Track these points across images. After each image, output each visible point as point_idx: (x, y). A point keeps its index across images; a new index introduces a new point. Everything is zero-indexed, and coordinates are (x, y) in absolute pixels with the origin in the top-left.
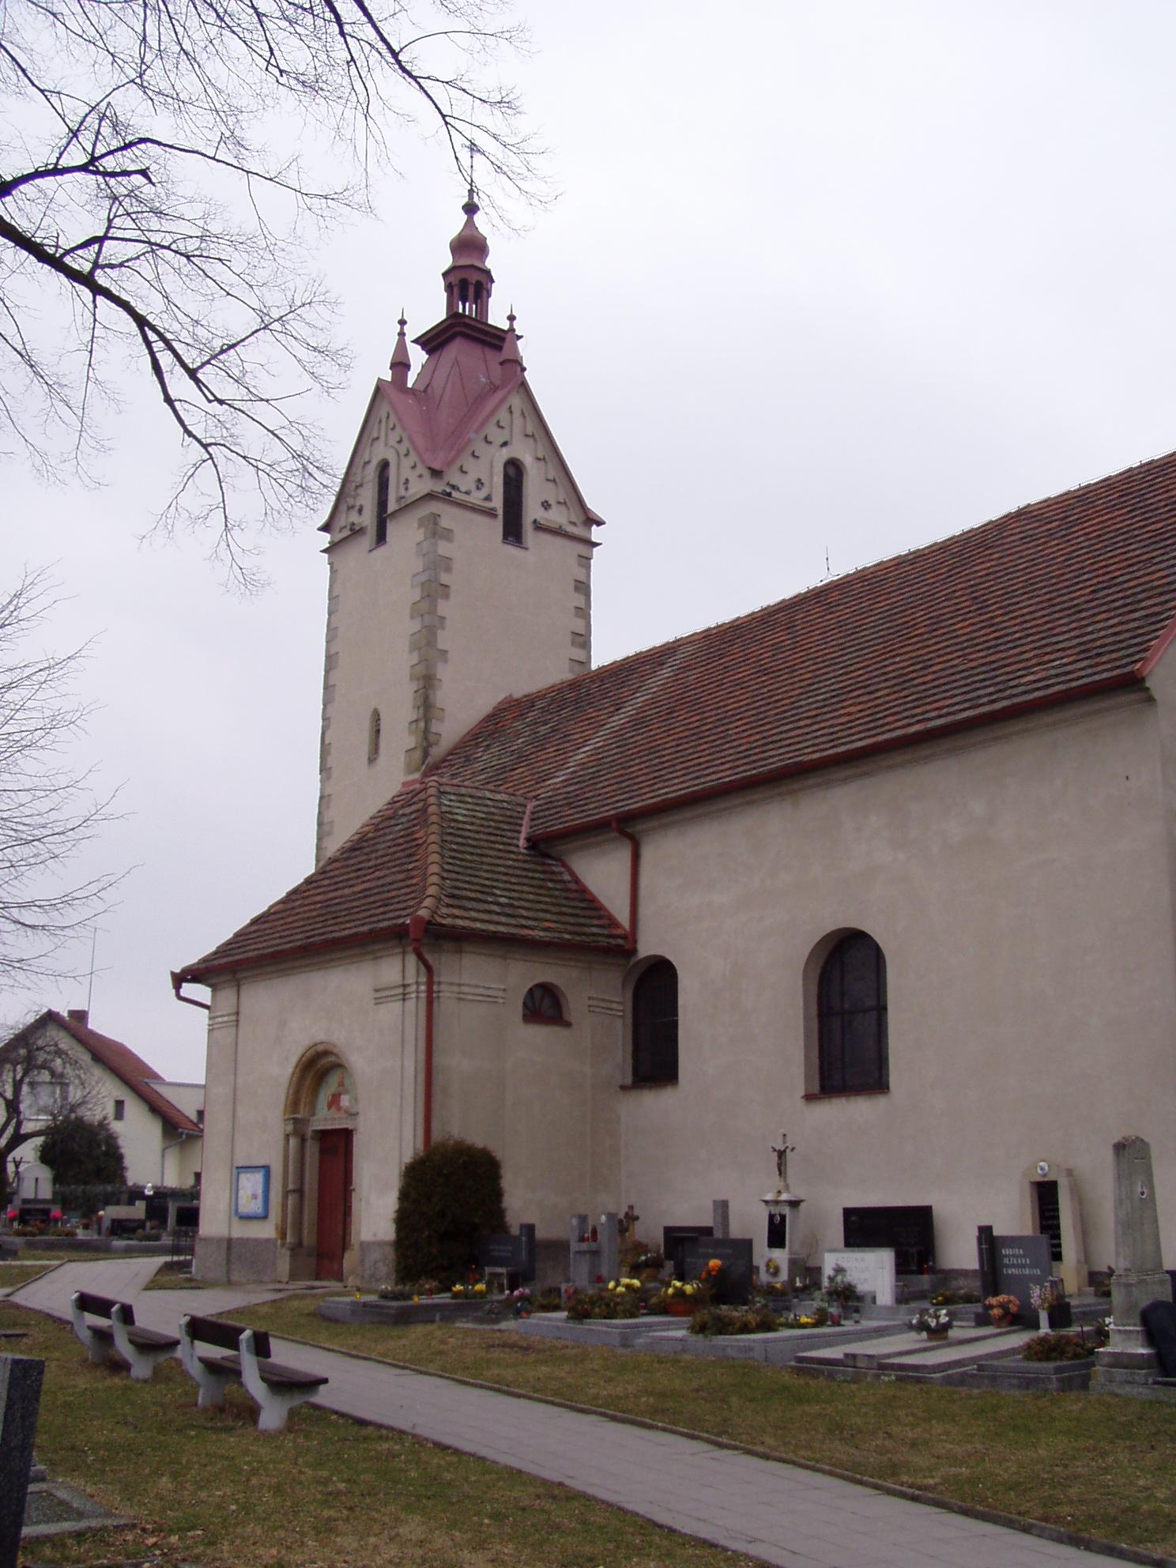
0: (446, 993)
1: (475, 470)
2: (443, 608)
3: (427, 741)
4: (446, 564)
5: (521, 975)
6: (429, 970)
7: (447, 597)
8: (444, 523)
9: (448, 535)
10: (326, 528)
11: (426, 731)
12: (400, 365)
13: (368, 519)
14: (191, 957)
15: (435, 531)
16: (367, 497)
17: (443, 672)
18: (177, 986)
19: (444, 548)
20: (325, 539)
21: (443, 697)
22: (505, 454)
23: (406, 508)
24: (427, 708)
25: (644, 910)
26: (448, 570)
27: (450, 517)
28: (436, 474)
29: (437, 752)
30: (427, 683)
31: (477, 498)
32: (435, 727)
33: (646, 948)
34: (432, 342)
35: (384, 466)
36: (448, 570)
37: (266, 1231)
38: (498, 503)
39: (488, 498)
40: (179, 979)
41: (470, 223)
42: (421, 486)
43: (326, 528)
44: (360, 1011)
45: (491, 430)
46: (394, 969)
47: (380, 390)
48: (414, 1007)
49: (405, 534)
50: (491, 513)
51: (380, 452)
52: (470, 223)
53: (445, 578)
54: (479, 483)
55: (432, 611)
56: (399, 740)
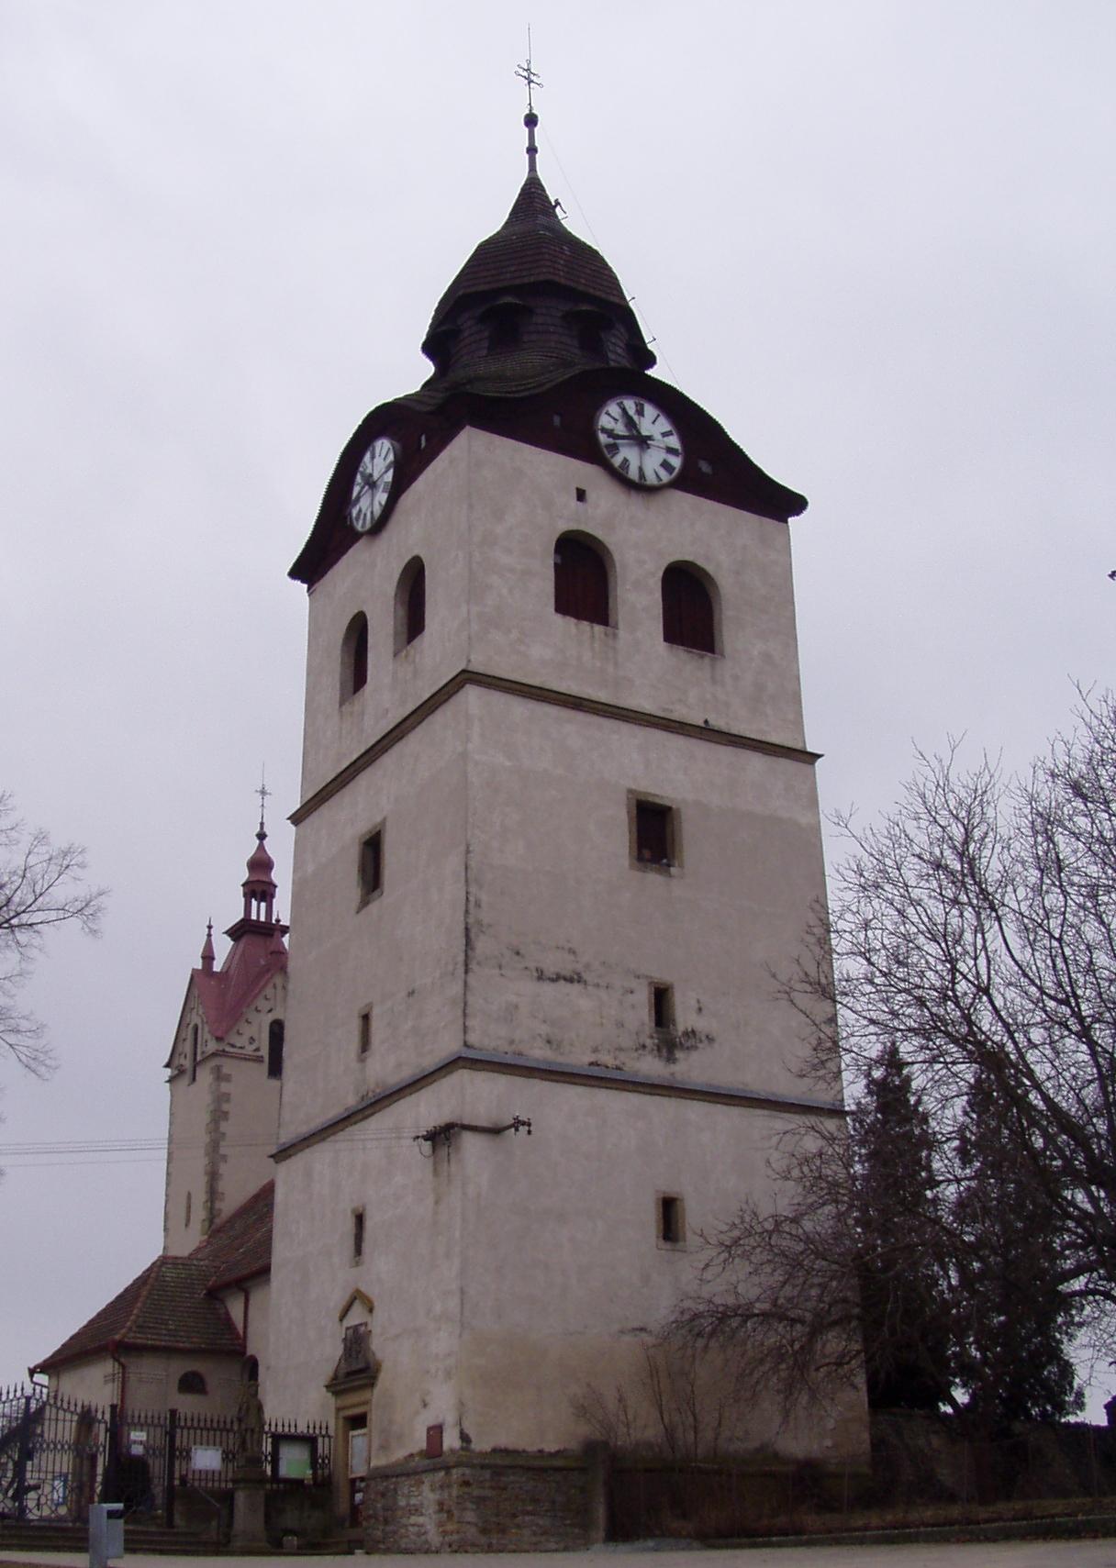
0: (132, 1379)
1: (248, 1031)
2: (224, 1127)
3: (212, 1214)
4: (226, 1097)
5: (179, 1367)
6: (123, 1367)
7: (226, 1119)
8: (225, 1070)
9: (228, 1078)
10: (167, 1066)
11: (212, 1209)
12: (208, 957)
13: (187, 1063)
14: (40, 1359)
15: (219, 1076)
16: (188, 1047)
17: (223, 1169)
18: (31, 1376)
19: (225, 1087)
20: (168, 1071)
21: (222, 1186)
22: (271, 1017)
23: (205, 1060)
24: (213, 1194)
25: (250, 1330)
26: (228, 1101)
27: (228, 1066)
28: (219, 1039)
29: (218, 1221)
30: (213, 1176)
31: (249, 1049)
32: (218, 1205)
33: (250, 1352)
34: (236, 933)
35: (196, 1029)
36: (228, 1101)
37: (63, 1511)
38: (265, 1052)
39: (257, 1050)
40: (32, 1372)
41: (261, 848)
42: (212, 1046)
43: (167, 1066)
44: (94, 1387)
45: (261, 1003)
46: (109, 1366)
47: (195, 974)
48: (117, 1385)
49: (205, 1076)
50: (259, 1060)
51: (195, 1019)
52: (261, 848)
53: (225, 1107)
54: (252, 1040)
55: (217, 1129)
56: (199, 1214)
